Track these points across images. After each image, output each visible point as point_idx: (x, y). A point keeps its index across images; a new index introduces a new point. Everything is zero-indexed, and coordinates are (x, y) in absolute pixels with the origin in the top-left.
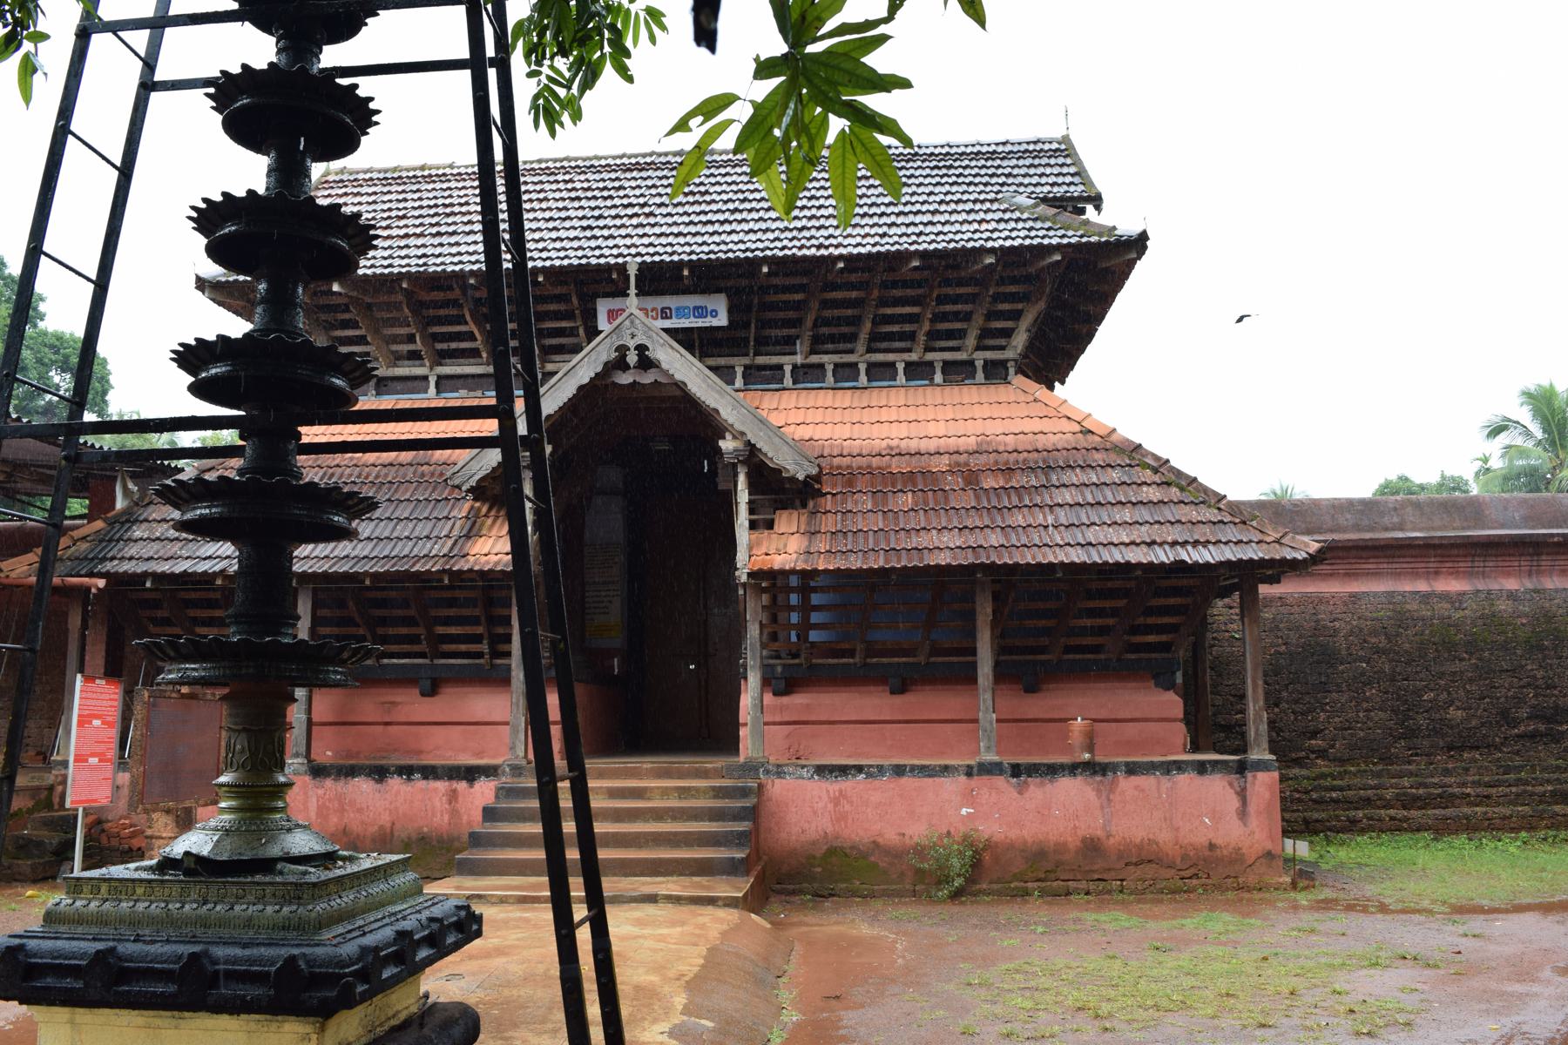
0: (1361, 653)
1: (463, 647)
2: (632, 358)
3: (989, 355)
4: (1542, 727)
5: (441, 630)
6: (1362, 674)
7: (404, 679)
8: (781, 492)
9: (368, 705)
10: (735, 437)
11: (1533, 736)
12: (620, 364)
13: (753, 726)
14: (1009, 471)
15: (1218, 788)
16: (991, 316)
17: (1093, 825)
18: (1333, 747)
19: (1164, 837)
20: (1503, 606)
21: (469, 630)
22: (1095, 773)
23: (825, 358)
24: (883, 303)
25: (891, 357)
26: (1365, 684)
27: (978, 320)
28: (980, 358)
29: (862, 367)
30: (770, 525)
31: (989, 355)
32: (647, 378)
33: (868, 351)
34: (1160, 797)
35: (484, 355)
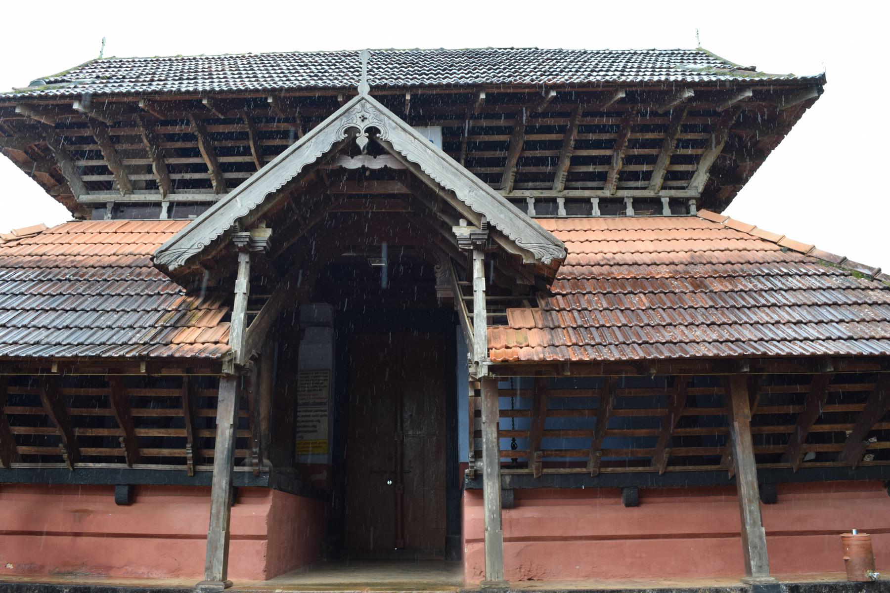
1: (166, 452)
2: (362, 141)
3: (674, 193)
5: (143, 432)
7: (99, 486)
8: (522, 284)
9: (59, 513)
10: (470, 224)
12: (348, 147)
13: (492, 544)
14: (731, 277)
16: (676, 160)
21: (172, 433)
23: (527, 193)
24: (581, 144)
25: (586, 193)
27: (665, 161)
28: (665, 196)
29: (561, 202)
30: (504, 321)
31: (674, 193)
32: (377, 164)
33: (566, 188)
35: (214, 183)
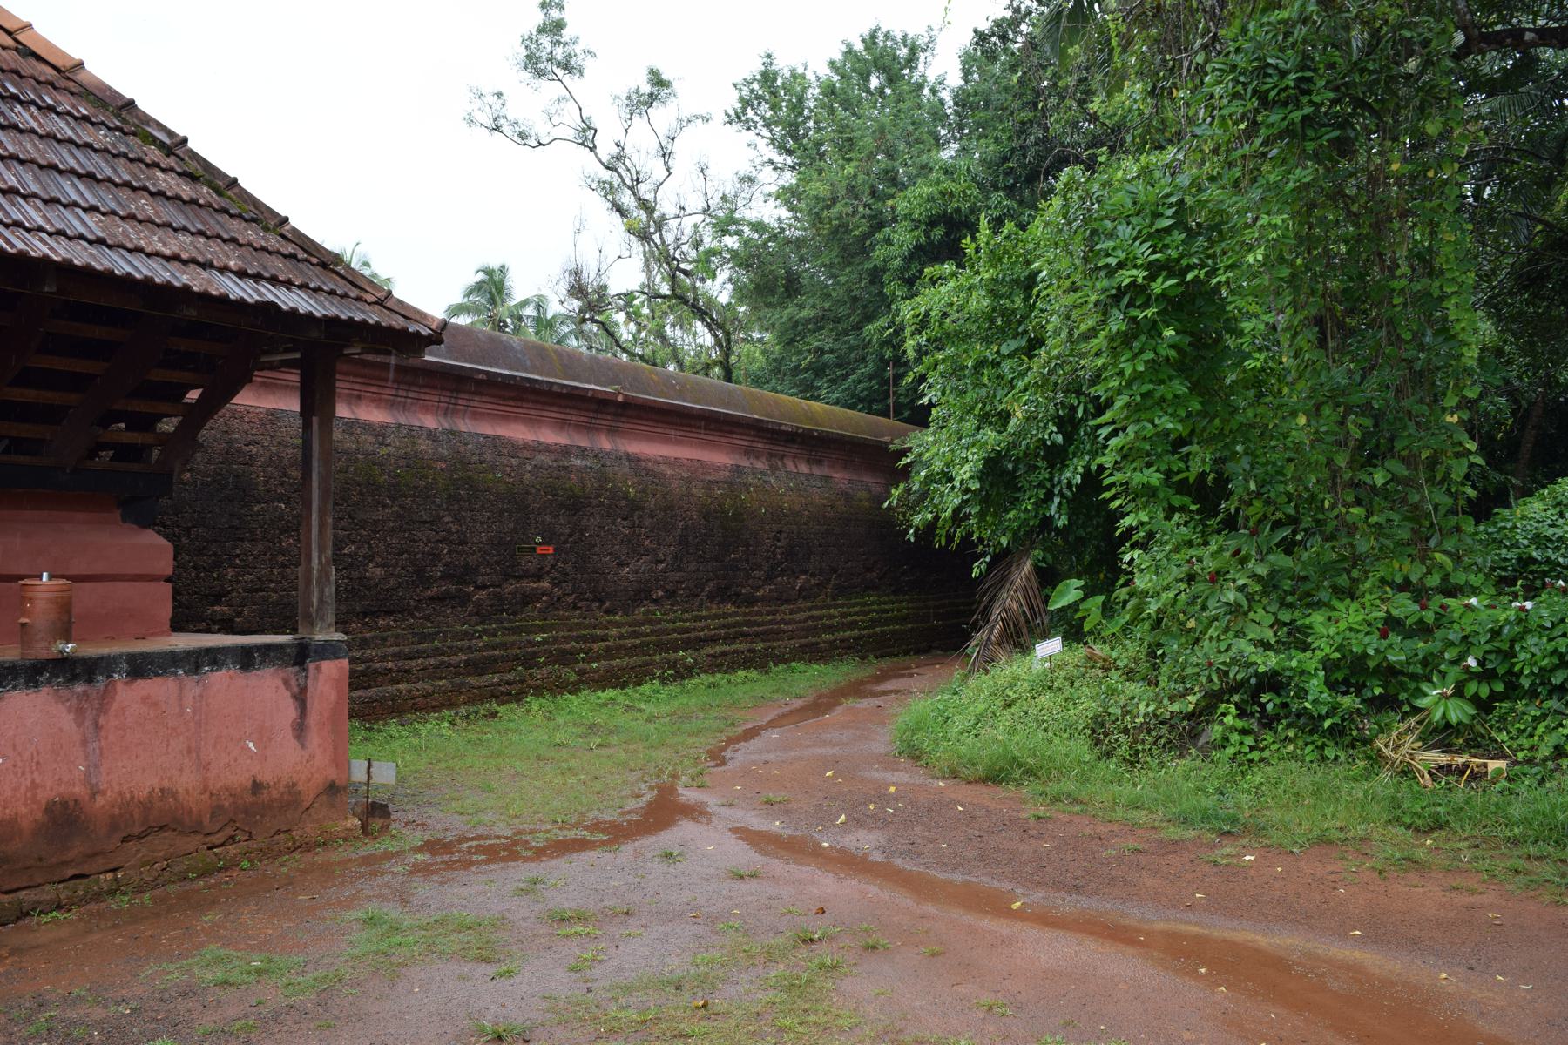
0: (280, 490)
4: (452, 588)
6: (281, 518)
11: (440, 599)
15: (267, 689)
17: (64, 777)
18: (239, 614)
19: (186, 782)
20: (424, 445)
22: (73, 679)
26: (283, 531)
34: (182, 713)
